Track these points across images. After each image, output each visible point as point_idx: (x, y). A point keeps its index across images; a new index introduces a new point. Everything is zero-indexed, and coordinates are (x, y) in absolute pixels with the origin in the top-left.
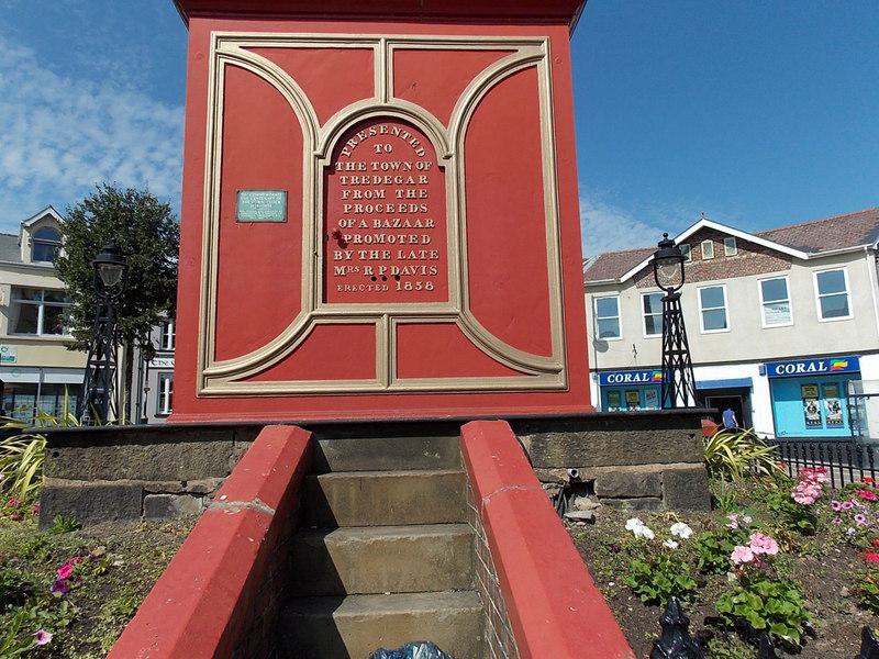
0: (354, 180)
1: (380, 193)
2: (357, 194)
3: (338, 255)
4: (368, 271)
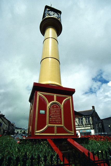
0: (52, 112)
1: (55, 112)
2: (52, 112)
3: (50, 118)
4: (53, 120)
